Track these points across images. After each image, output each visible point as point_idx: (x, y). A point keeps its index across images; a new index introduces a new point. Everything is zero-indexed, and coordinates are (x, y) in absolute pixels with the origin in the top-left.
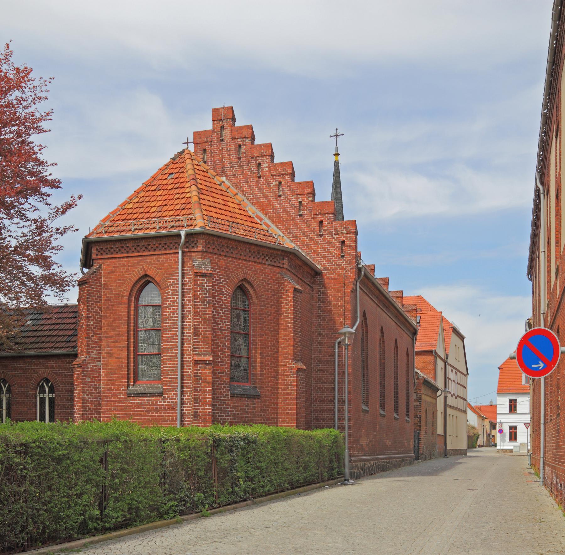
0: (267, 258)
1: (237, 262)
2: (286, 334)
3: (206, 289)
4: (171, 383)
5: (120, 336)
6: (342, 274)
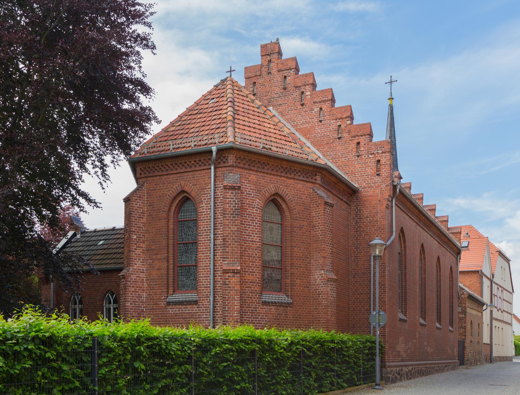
0: (299, 174)
1: (268, 177)
2: (318, 246)
3: (235, 201)
4: (205, 292)
5: (161, 249)
6: (378, 191)
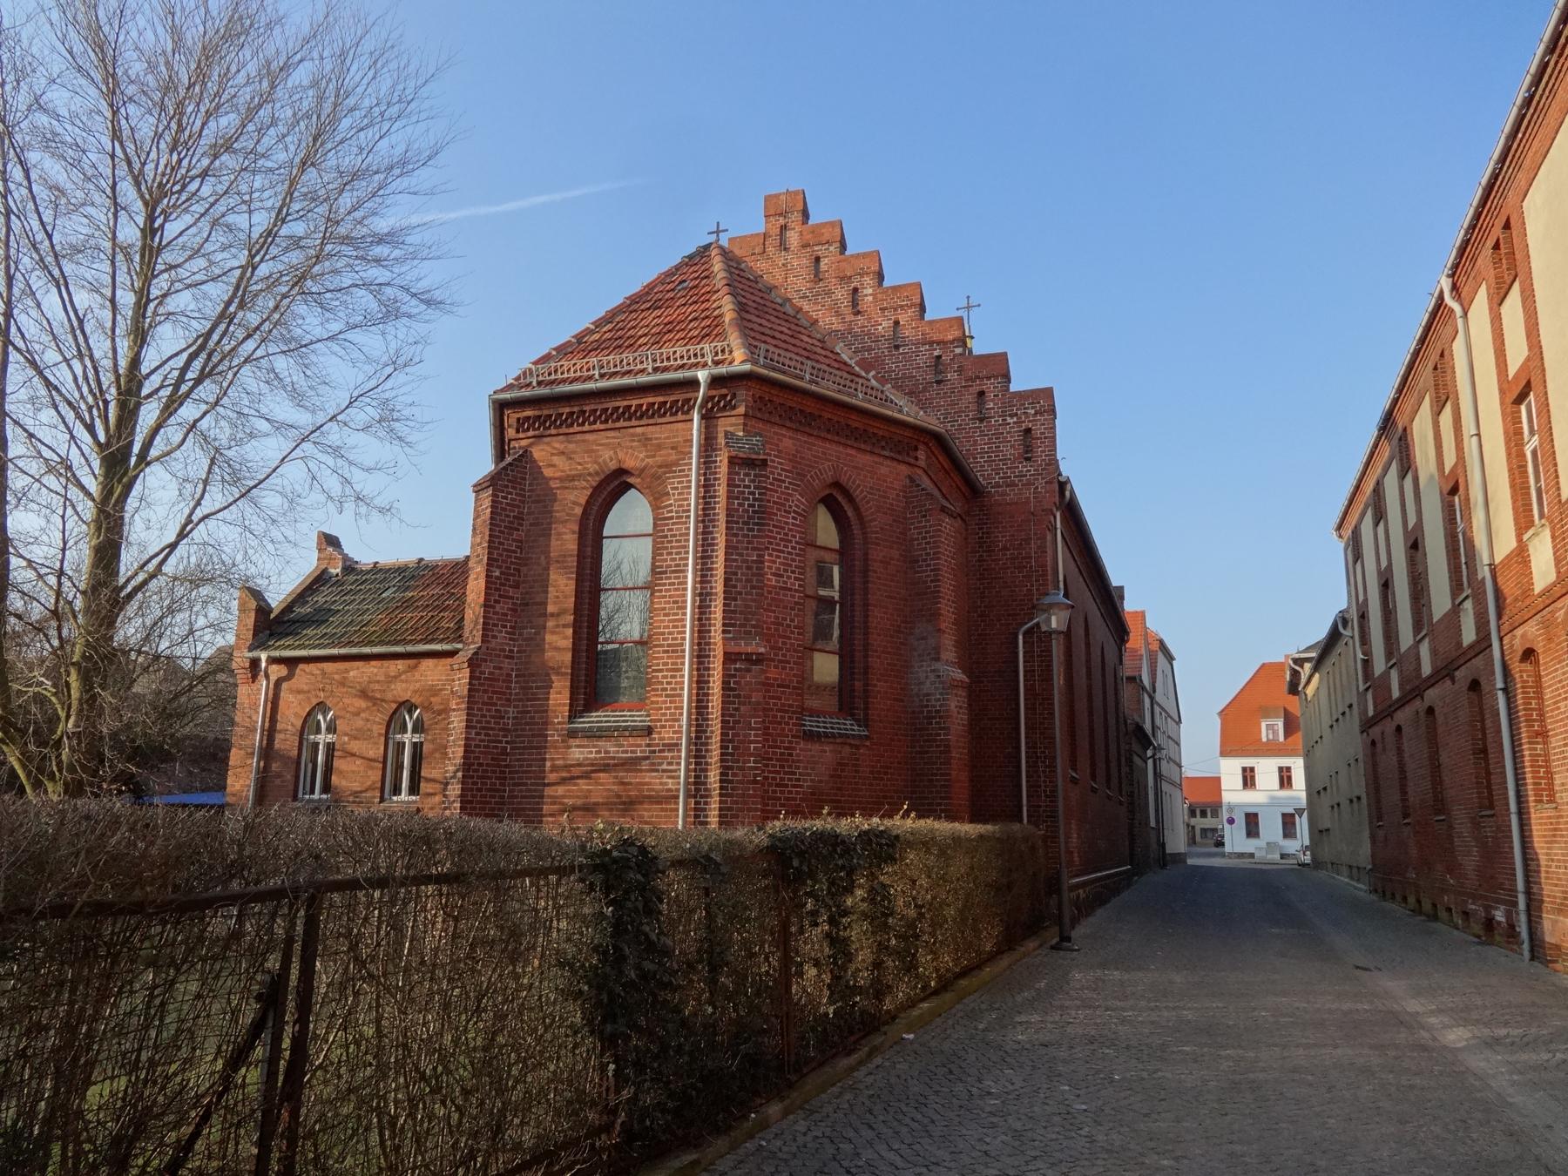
6: (1029, 493)
